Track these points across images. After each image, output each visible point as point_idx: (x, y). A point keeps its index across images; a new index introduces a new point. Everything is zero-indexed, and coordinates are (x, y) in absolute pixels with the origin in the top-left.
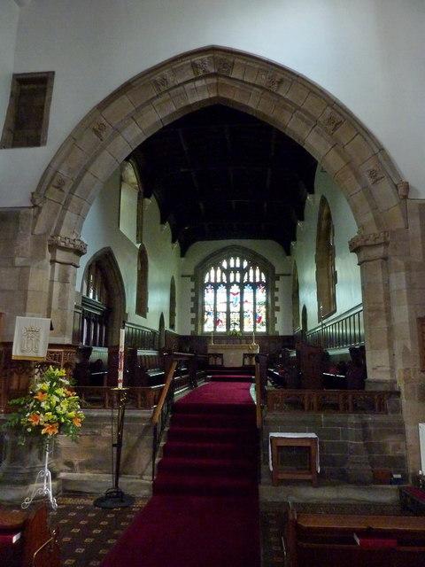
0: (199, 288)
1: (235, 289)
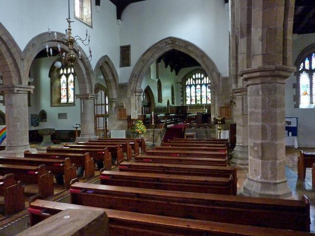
0: (184, 87)
1: (198, 87)
